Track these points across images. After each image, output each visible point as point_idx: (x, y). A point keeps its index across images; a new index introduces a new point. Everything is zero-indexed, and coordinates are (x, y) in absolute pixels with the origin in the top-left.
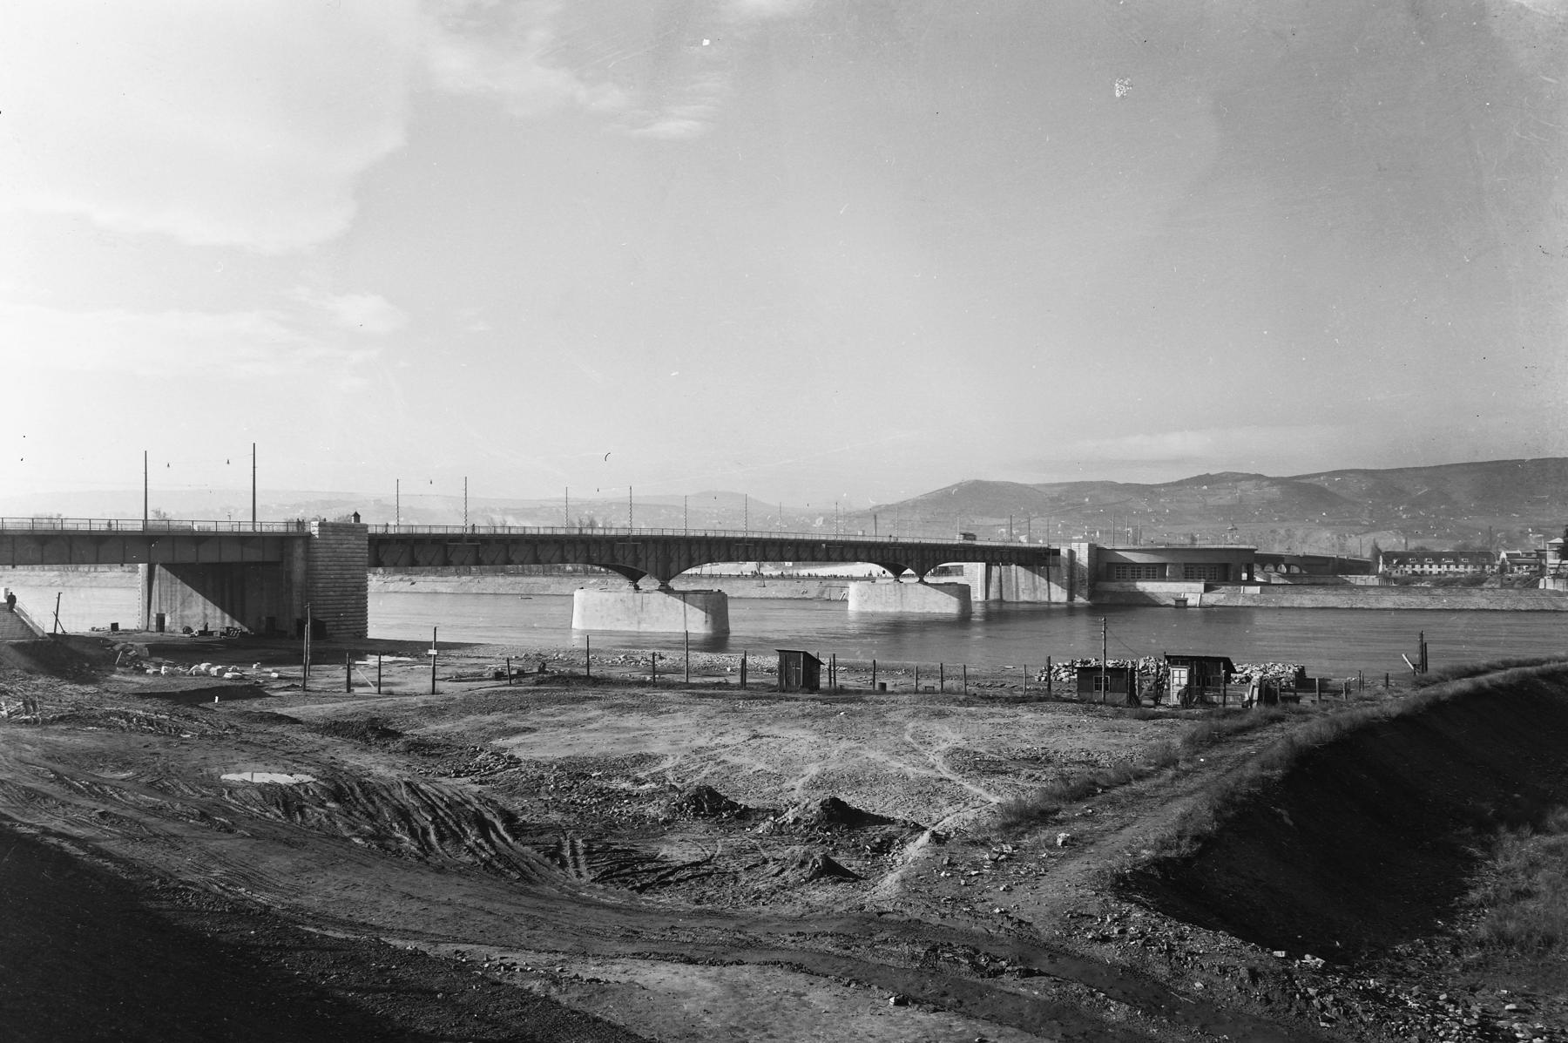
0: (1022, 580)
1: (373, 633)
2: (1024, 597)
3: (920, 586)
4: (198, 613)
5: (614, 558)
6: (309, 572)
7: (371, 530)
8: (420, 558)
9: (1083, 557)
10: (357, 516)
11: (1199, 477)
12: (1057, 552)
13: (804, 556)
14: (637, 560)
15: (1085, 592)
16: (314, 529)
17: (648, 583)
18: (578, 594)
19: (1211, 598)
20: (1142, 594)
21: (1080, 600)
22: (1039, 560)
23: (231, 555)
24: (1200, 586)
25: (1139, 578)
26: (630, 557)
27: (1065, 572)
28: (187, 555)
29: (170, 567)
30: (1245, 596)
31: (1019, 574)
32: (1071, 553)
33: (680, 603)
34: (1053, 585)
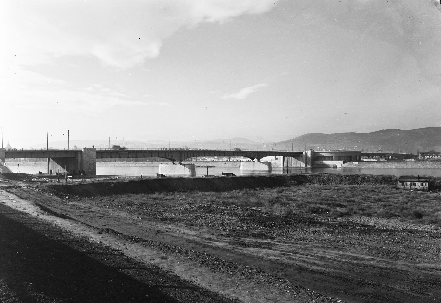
0: (293, 161)
1: (97, 174)
2: (294, 166)
3: (258, 163)
4: (59, 169)
5: (166, 156)
6: (82, 160)
7: (97, 150)
8: (113, 156)
9: (309, 154)
10: (93, 146)
11: (380, 131)
12: (302, 153)
13: (235, 155)
14: (172, 156)
15: (310, 164)
16: (83, 150)
17: (177, 162)
18: (160, 165)
19: (344, 165)
20: (325, 164)
21: (309, 166)
22: (297, 155)
23: (64, 156)
24: (342, 162)
25: (326, 160)
26: (170, 155)
27: (304, 158)
28: (58, 156)
29: (53, 158)
30: (354, 165)
31: (292, 159)
32: (306, 153)
33: (184, 167)
34: (301, 163)
